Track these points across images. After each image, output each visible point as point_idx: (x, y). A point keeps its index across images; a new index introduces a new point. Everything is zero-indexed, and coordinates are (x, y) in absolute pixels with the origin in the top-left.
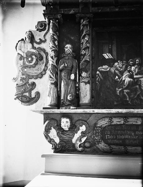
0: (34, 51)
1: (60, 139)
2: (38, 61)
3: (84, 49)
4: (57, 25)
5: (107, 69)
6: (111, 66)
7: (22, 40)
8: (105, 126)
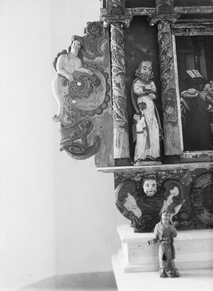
1: (142, 212)
2: (93, 87)
4: (122, 32)
5: (194, 94)
6: (201, 89)
7: (64, 52)
8: (205, 186)
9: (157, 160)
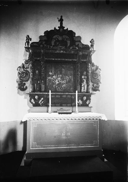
0: (24, 71)
3: (43, 73)
9: (86, 92)
